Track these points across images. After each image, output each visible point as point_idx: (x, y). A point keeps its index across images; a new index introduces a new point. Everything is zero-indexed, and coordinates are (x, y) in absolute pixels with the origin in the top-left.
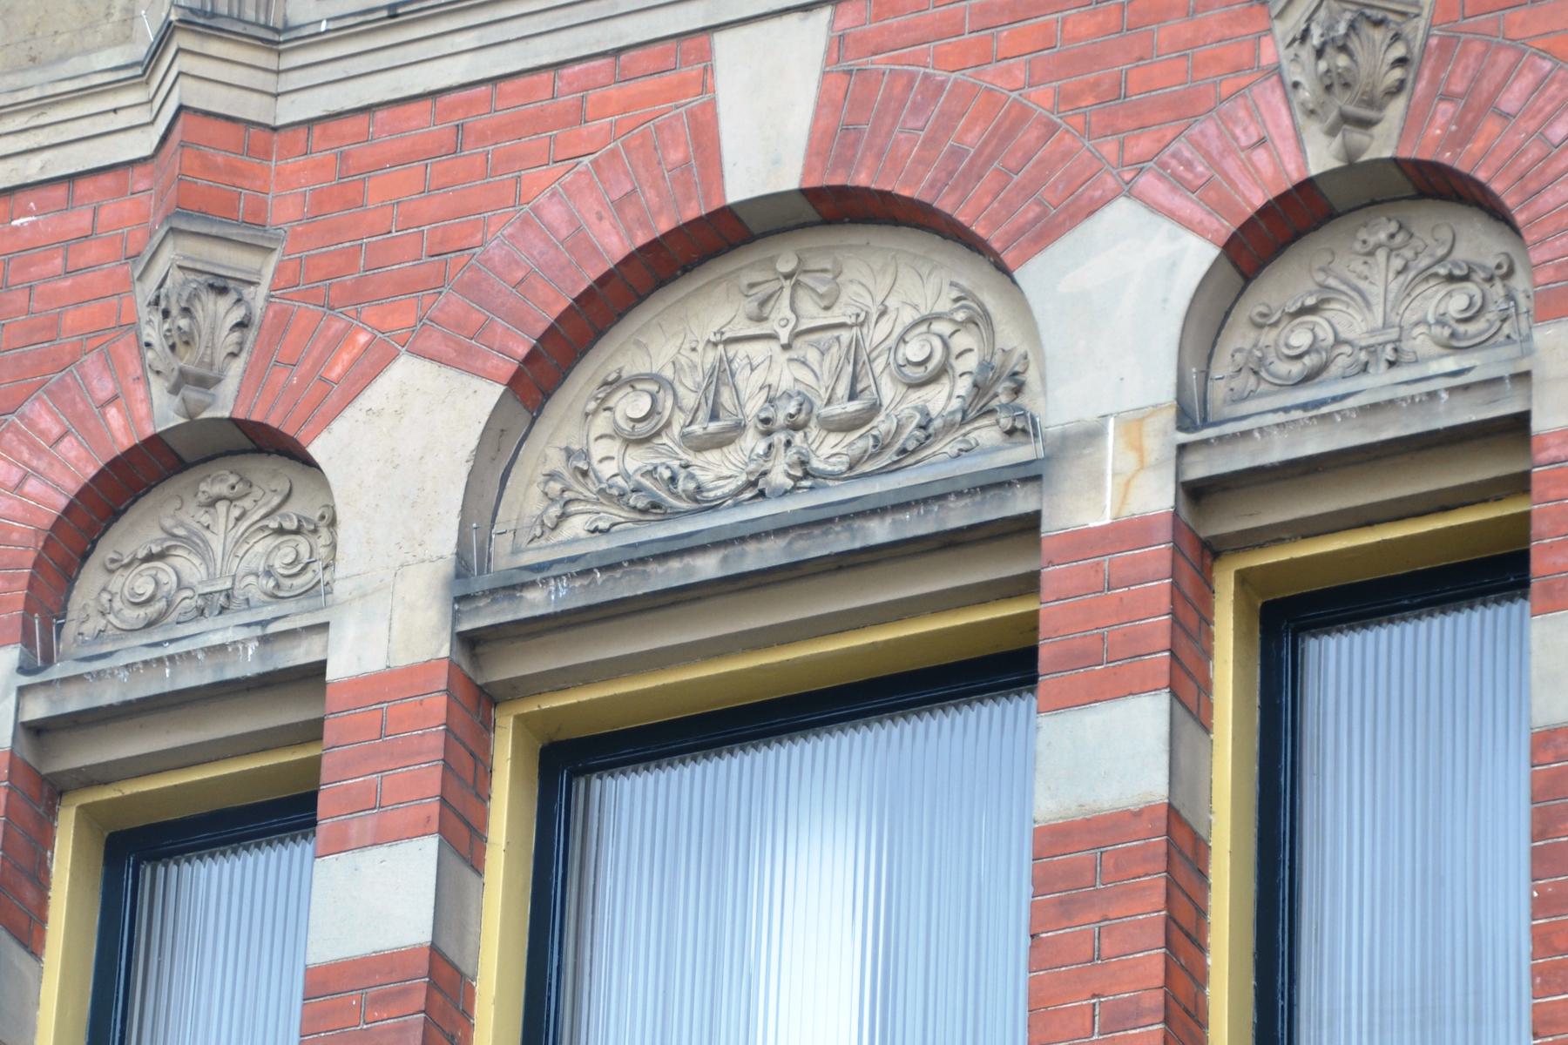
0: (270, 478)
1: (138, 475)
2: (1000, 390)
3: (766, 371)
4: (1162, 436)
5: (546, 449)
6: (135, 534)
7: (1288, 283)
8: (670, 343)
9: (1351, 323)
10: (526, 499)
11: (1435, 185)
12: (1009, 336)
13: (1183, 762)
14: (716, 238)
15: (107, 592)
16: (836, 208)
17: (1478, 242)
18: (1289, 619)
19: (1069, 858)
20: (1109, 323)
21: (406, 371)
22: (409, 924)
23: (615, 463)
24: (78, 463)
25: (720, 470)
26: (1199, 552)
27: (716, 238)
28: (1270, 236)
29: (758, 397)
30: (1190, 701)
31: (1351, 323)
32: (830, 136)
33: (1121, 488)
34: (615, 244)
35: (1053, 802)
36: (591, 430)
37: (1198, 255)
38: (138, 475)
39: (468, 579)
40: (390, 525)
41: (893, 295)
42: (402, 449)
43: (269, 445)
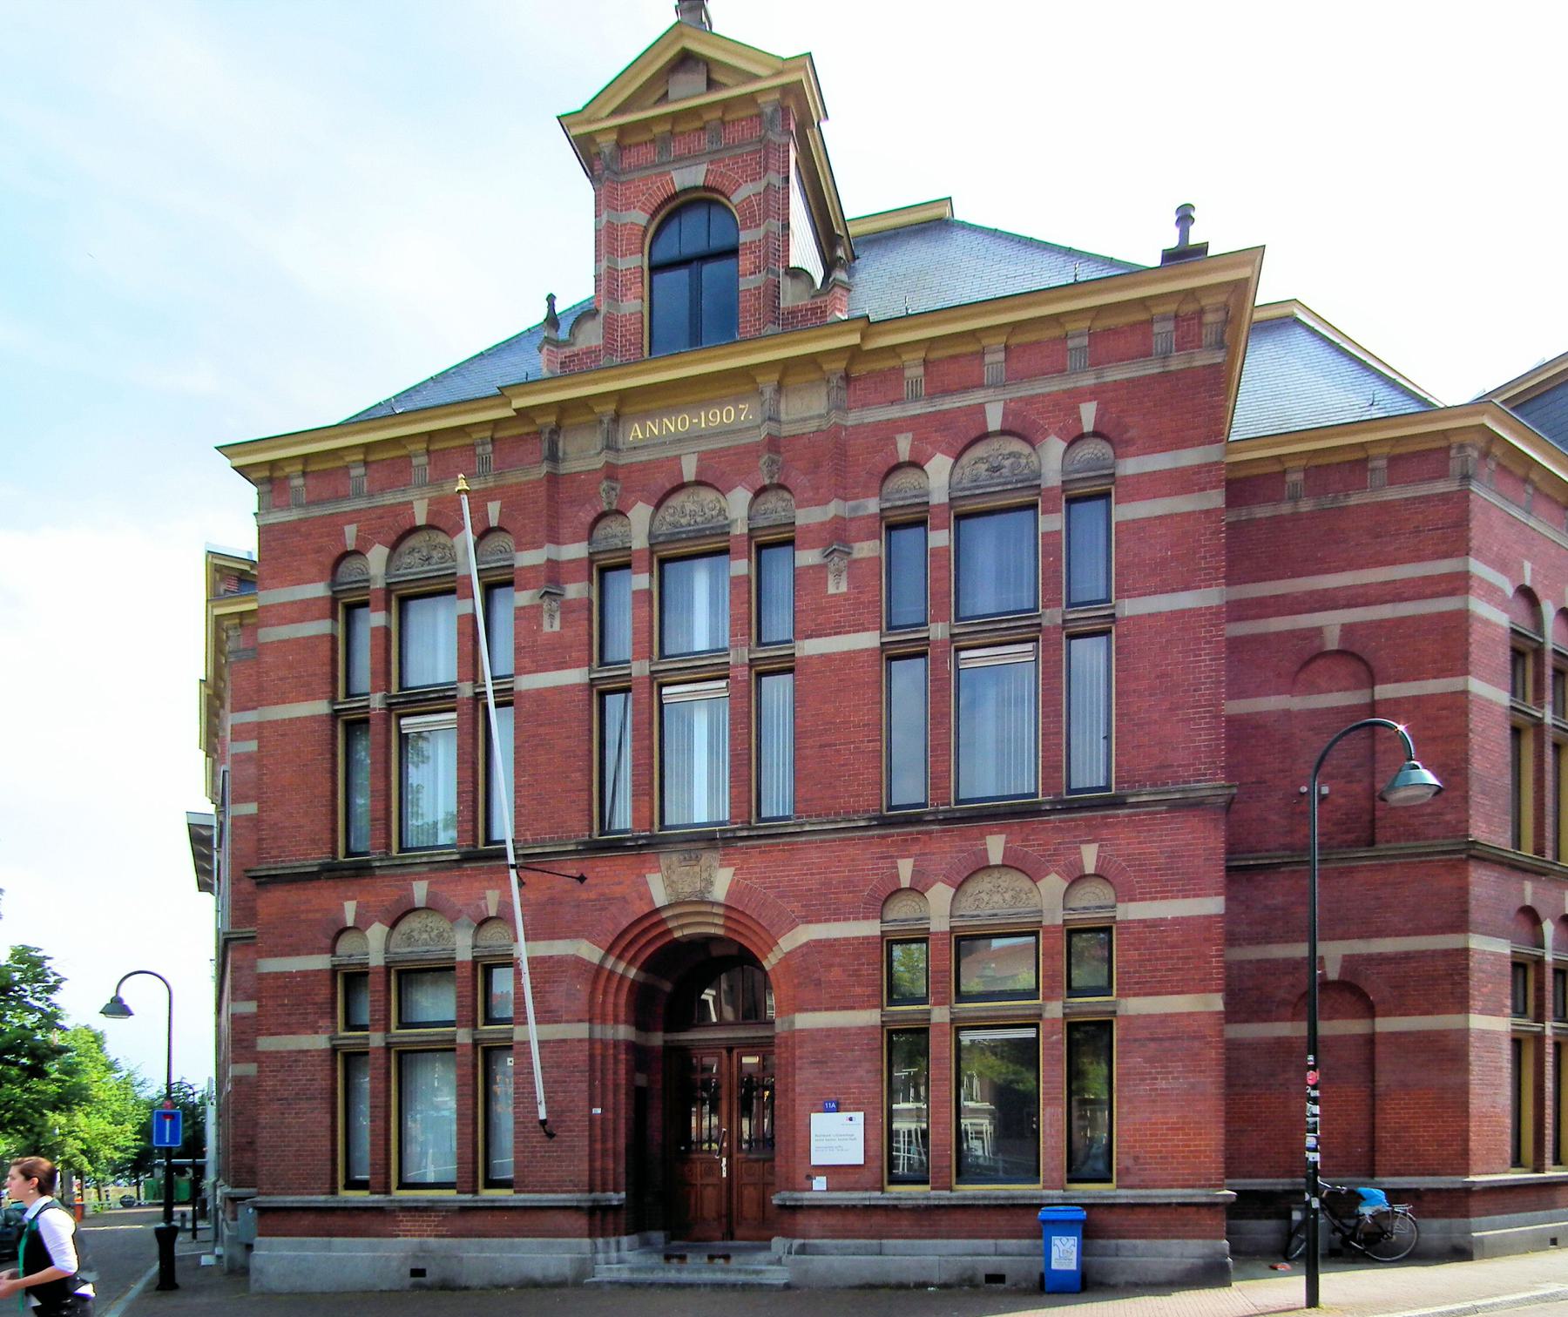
0: (620, 518)
1: (602, 516)
2: (722, 511)
3: (689, 507)
4: (746, 521)
5: (659, 517)
6: (600, 525)
7: (762, 499)
8: (677, 501)
9: (769, 506)
10: (657, 522)
11: (781, 487)
12: (723, 504)
13: (334, 627)
14: (898, 467)
15: (600, 532)
16: (699, 483)
17: (786, 495)
18: (761, 547)
19: (735, 582)
20: (738, 504)
21: (640, 504)
22: (745, 571)
23: (668, 519)
24: (594, 515)
25: (684, 521)
26: (750, 538)
27: (682, 486)
28: (760, 492)
29: (691, 509)
30: (591, 581)
31: (769, 506)
32: (698, 473)
33: (740, 529)
34: (668, 486)
35: (635, 588)
36: (667, 514)
37: (750, 495)
38: (602, 516)
39: (651, 535)
40: (638, 525)
41: (708, 496)
42: (640, 514)
43: (622, 514)
